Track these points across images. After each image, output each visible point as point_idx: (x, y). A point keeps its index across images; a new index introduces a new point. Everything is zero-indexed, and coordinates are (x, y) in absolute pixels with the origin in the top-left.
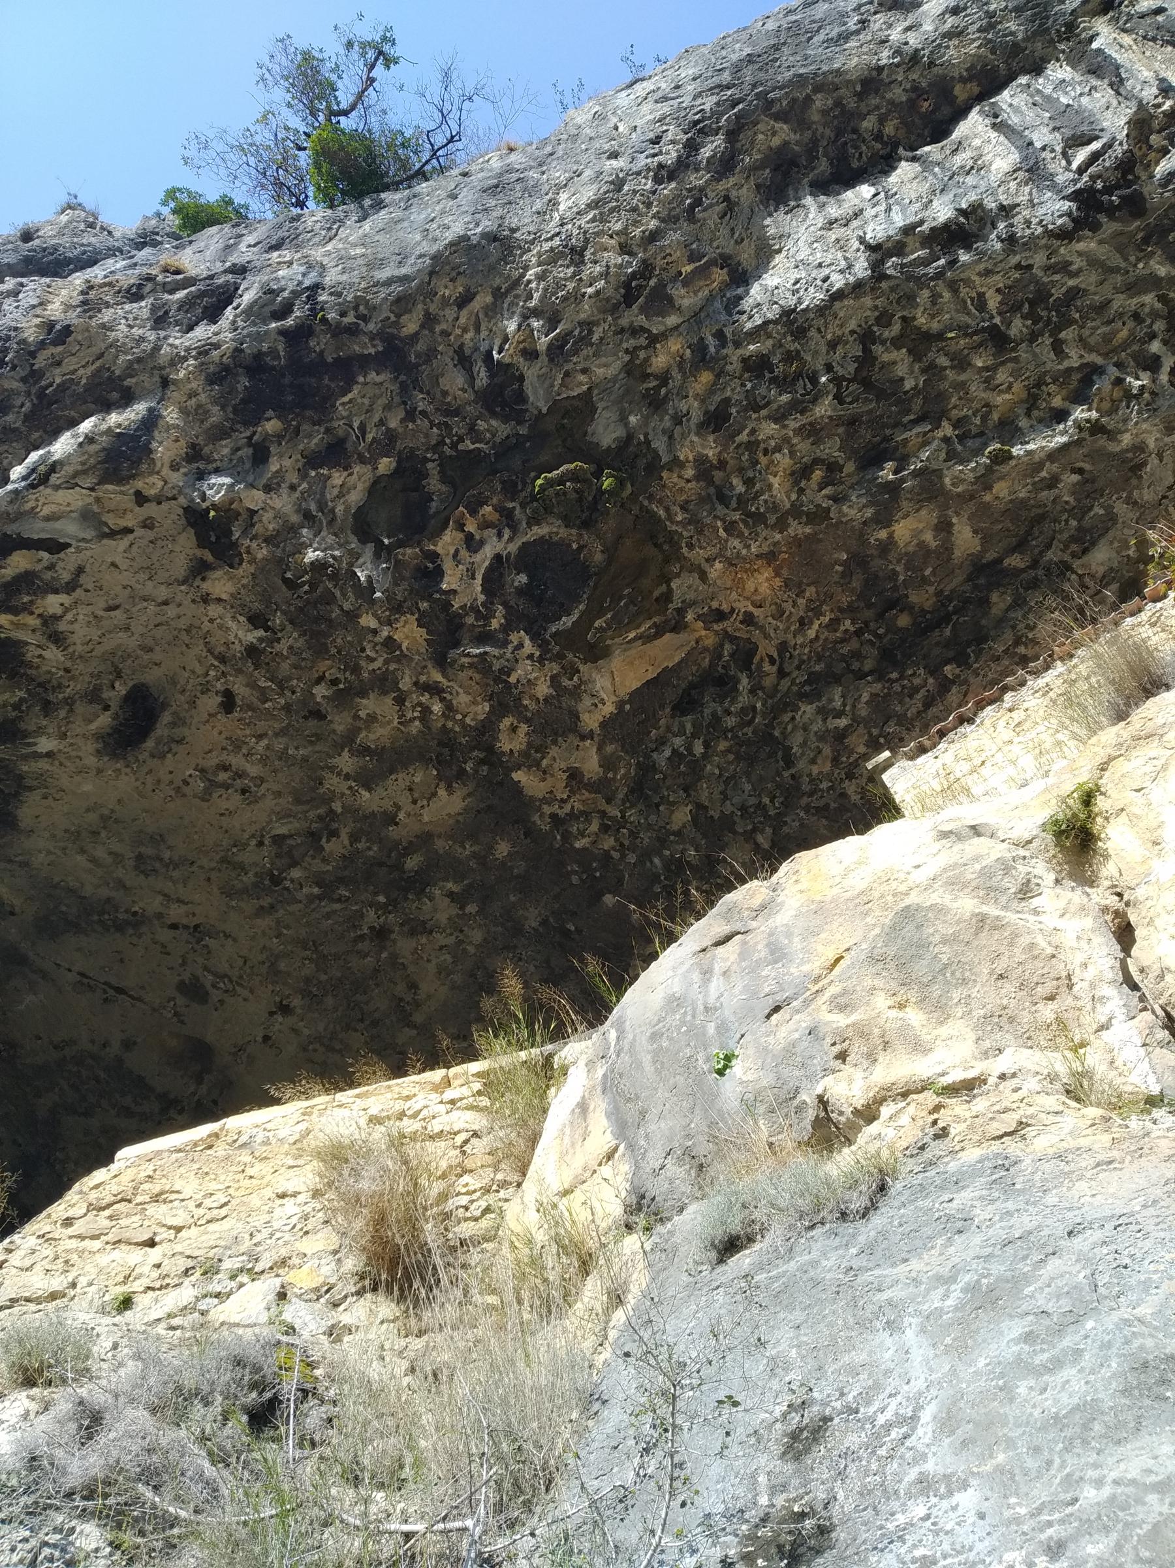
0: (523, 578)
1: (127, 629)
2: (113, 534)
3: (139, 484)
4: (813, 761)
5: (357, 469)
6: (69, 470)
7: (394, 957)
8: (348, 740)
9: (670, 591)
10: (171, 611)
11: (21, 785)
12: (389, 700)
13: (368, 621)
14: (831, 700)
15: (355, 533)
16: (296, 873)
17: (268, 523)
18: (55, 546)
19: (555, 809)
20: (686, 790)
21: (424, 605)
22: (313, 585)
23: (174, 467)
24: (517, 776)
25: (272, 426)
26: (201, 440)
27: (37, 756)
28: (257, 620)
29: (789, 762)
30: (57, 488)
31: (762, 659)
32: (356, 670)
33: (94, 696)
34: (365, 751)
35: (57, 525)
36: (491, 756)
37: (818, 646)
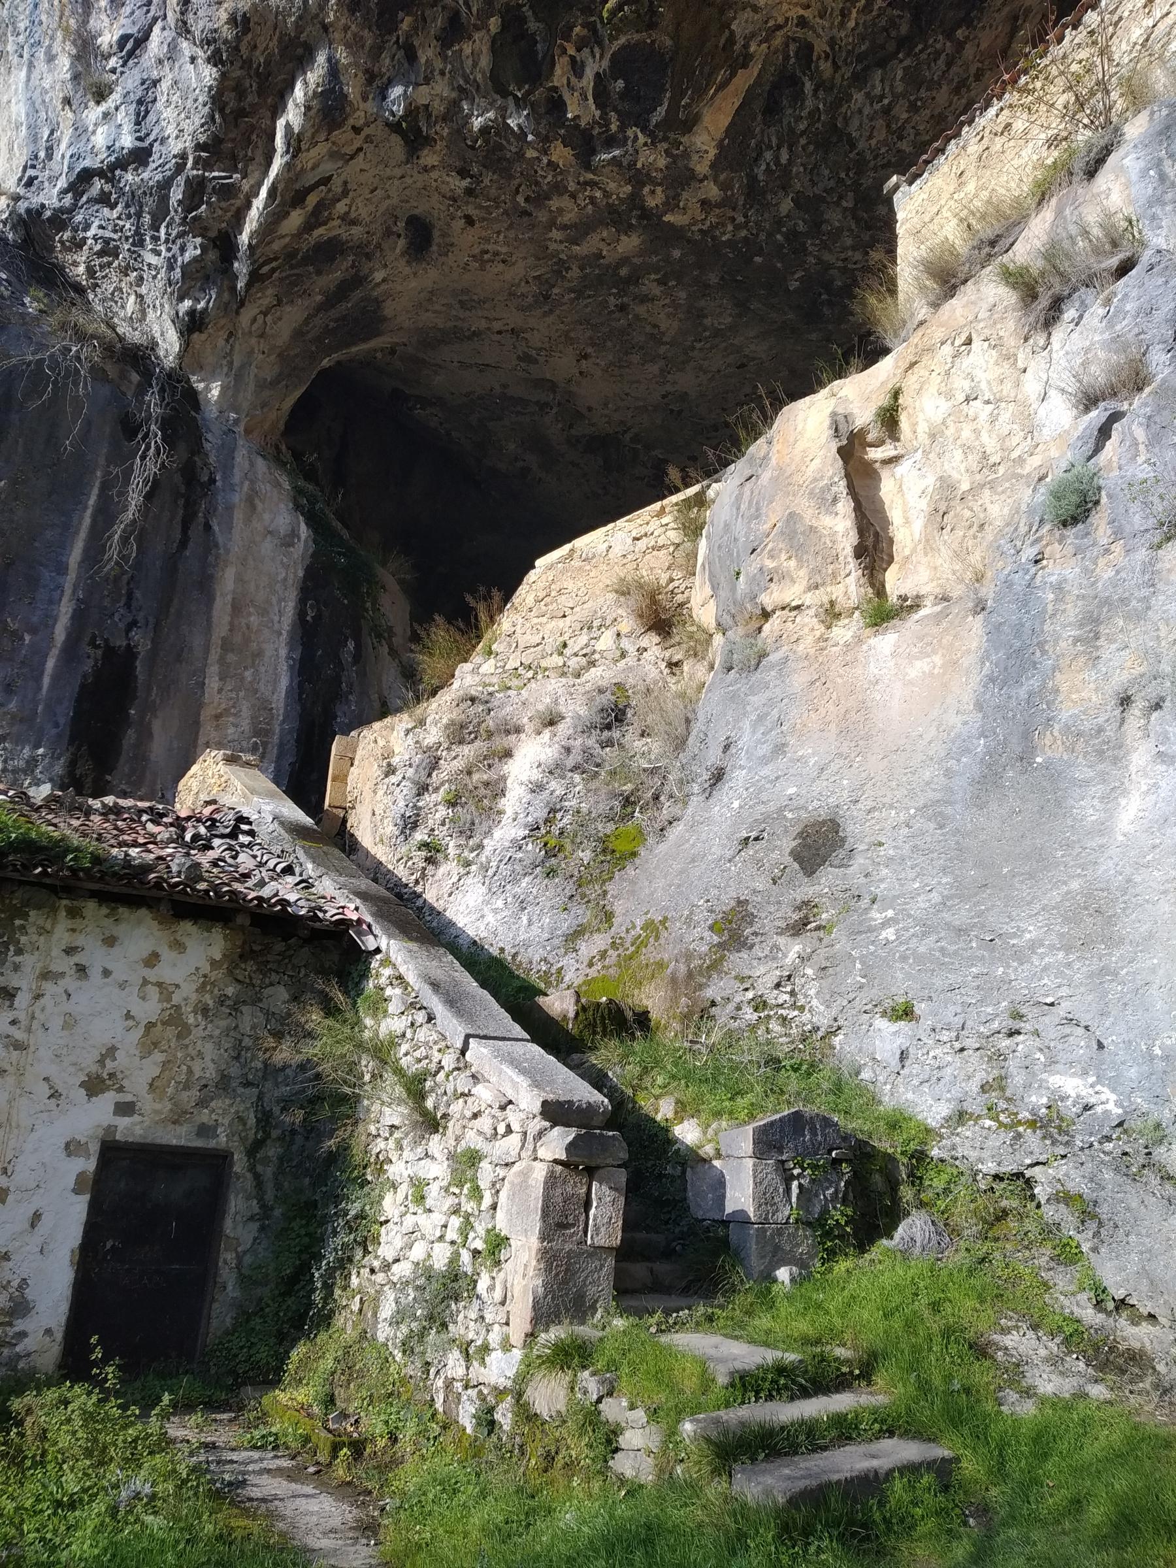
0: (620, 84)
1: (389, 197)
2: (352, 157)
3: (351, 121)
4: (870, 137)
5: (477, 36)
6: (309, 134)
7: (637, 317)
8: (552, 224)
9: (732, 33)
10: (409, 181)
11: (378, 302)
12: (566, 197)
13: (531, 154)
14: (873, 87)
15: (497, 92)
16: (556, 291)
17: (438, 108)
18: (326, 181)
19: (700, 226)
20: (784, 188)
21: (562, 132)
22: (487, 142)
23: (365, 99)
24: (666, 218)
25: (406, 25)
26: (369, 65)
27: (378, 285)
28: (463, 173)
29: (852, 145)
30: (308, 150)
31: (819, 58)
32: (537, 183)
33: (388, 233)
34: (564, 227)
35: (320, 169)
36: (646, 214)
37: (861, 29)
